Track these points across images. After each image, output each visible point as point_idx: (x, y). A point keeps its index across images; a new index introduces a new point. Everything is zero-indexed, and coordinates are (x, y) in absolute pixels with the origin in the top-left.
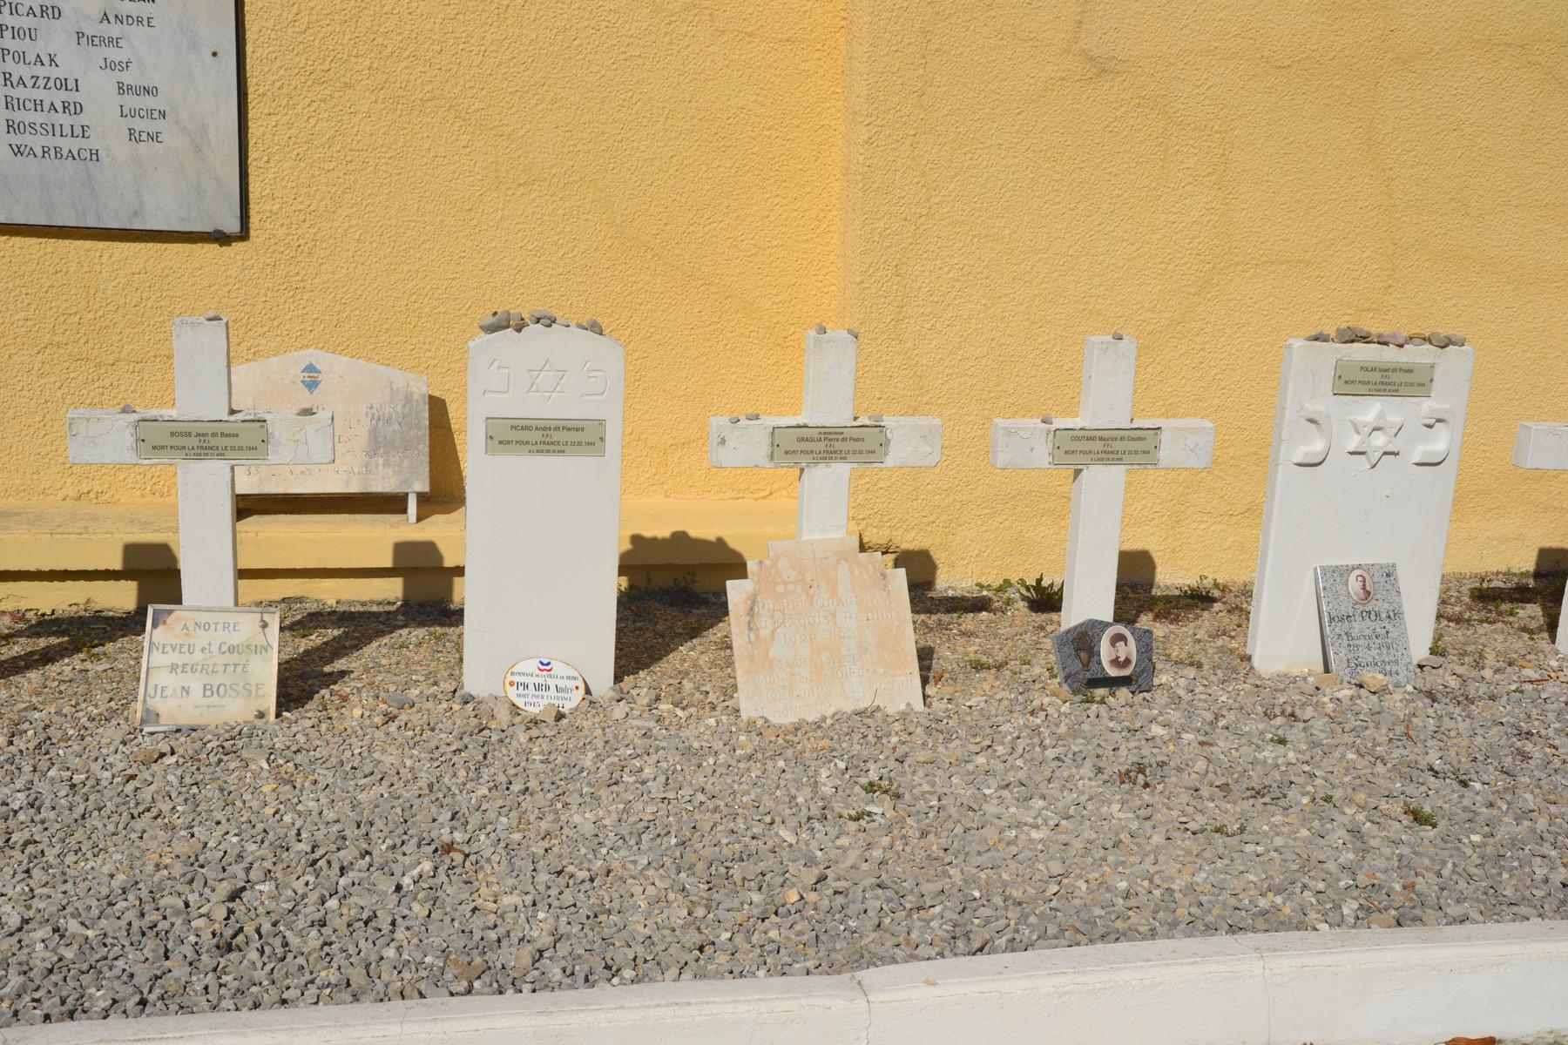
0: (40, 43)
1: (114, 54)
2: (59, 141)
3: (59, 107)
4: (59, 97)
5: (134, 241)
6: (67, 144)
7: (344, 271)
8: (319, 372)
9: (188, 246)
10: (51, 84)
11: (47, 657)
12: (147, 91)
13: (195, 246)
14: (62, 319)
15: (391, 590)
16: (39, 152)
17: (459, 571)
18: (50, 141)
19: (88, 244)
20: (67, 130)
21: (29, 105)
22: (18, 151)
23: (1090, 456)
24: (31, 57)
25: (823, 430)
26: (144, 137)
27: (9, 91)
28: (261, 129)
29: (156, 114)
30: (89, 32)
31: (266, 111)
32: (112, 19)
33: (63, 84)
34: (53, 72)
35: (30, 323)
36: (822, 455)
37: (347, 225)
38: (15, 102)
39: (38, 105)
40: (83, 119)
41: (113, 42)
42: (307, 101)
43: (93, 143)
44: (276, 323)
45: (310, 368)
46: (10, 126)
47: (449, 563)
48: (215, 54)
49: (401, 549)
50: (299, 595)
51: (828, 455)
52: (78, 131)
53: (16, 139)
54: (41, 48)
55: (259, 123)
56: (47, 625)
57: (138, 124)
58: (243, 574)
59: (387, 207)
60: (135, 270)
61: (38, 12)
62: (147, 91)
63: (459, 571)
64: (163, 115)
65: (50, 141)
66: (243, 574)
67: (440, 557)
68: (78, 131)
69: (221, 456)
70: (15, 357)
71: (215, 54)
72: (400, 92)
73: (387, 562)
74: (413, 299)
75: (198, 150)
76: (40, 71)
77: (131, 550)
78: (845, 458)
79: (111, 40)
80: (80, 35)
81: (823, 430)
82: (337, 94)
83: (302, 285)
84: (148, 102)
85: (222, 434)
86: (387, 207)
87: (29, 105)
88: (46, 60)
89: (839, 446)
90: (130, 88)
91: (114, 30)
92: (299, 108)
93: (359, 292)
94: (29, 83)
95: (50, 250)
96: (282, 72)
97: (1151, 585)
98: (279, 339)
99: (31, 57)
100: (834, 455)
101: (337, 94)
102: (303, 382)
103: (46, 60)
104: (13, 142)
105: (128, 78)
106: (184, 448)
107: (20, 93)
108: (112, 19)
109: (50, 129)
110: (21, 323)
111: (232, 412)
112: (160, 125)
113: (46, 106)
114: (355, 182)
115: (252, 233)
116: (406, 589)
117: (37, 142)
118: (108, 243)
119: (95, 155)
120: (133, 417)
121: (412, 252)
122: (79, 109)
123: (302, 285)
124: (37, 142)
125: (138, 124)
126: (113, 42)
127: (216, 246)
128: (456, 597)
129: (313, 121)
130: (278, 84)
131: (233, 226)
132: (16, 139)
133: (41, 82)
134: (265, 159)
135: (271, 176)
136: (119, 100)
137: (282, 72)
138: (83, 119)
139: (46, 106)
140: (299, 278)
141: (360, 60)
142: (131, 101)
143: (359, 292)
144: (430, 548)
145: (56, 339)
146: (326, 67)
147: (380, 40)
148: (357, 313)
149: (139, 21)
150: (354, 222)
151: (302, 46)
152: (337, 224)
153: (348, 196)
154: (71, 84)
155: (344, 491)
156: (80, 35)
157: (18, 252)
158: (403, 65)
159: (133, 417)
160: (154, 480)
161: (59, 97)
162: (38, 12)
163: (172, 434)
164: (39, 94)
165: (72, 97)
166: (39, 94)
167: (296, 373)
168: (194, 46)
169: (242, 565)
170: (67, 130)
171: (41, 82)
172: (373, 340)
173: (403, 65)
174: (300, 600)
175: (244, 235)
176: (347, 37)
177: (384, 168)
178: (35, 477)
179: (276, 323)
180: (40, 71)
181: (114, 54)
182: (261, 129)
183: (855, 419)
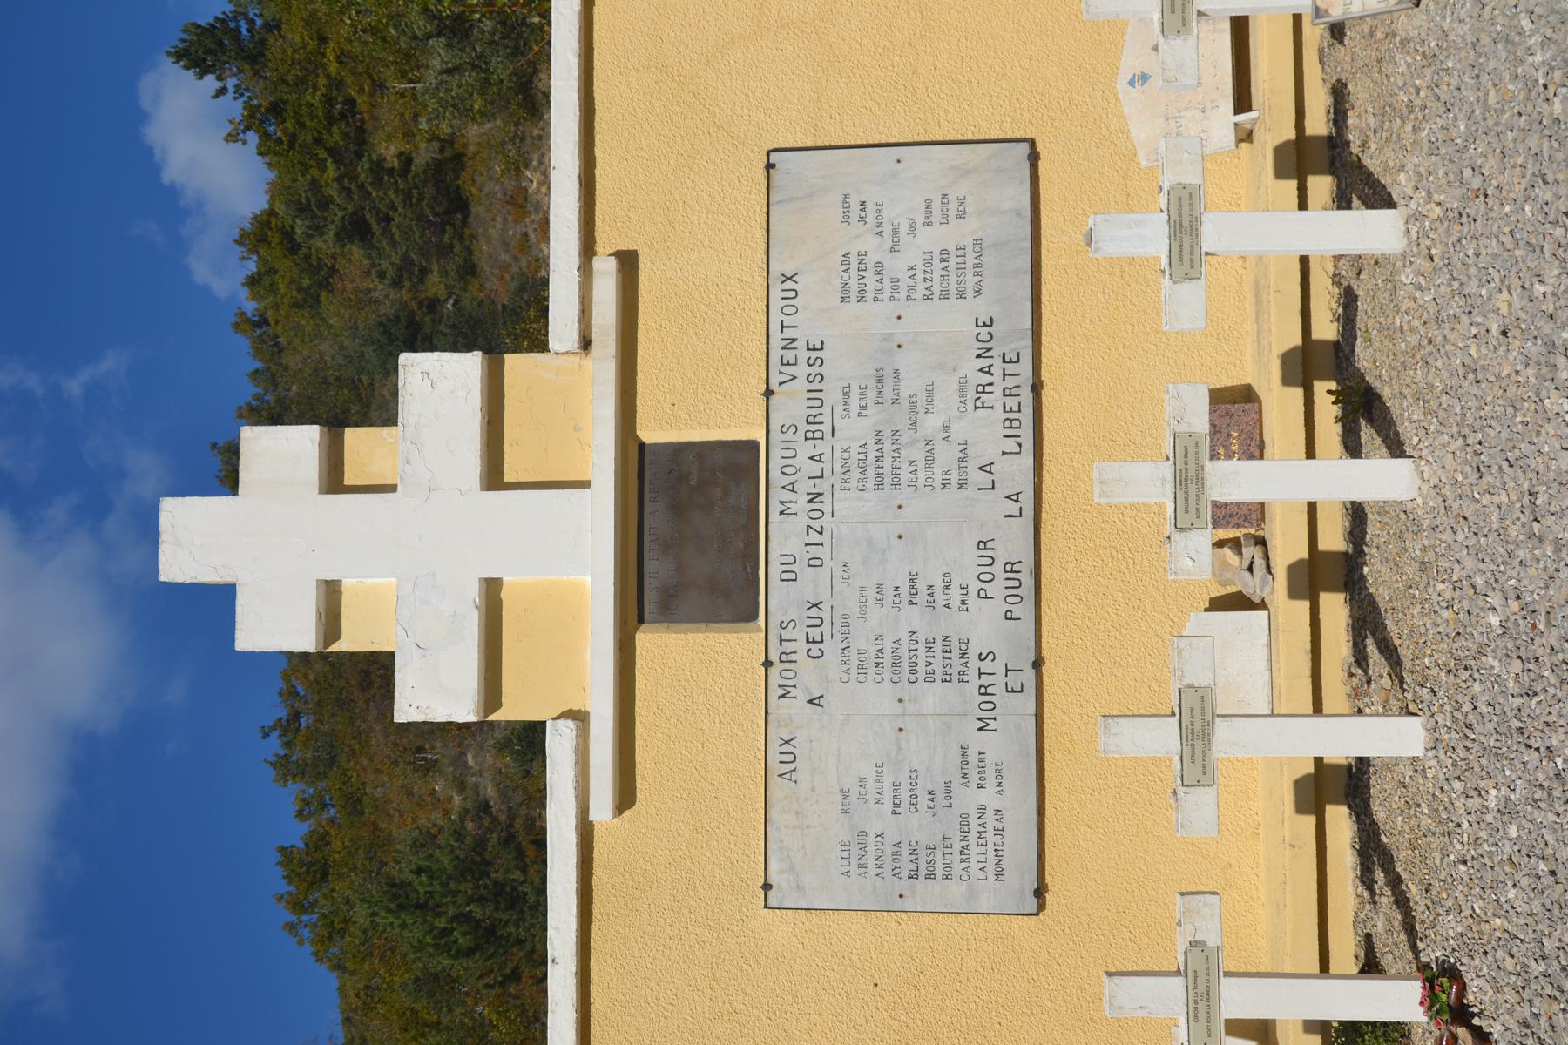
0: (900, 276)
1: (904, 229)
2: (969, 265)
3: (945, 264)
4: (937, 265)
5: (1039, 219)
6: (971, 260)
7: (1055, 69)
8: (1134, 75)
9: (1041, 182)
10: (928, 270)
11: (1395, 882)
12: (928, 206)
13: (1041, 178)
14: (1101, 269)
15: (1340, 820)
16: (978, 278)
17: (1318, 761)
18: (970, 272)
19: (1044, 251)
20: (961, 260)
21: (945, 284)
22: (978, 292)
23: (1195, 246)
24: (911, 282)
25: (1173, 238)
26: (961, 208)
27: (936, 296)
28: (951, 131)
29: (945, 201)
30: (890, 244)
31: (937, 128)
32: (880, 229)
33: (929, 262)
34: (920, 267)
35: (1106, 290)
36: (1206, 742)
37: (1019, 68)
38: (943, 293)
39: (944, 278)
40: (952, 249)
41: (895, 229)
42: (928, 99)
43: (969, 242)
44: (1098, 118)
45: (1132, 83)
46: (961, 296)
47: (1311, 769)
48: (899, 161)
49: (1293, 594)
50: (1316, 52)
51: (1200, 482)
52: (961, 253)
53: (970, 293)
54: (904, 276)
55: (946, 133)
56: (1367, 880)
57: (953, 212)
58: (1318, 709)
59: (1003, 39)
60: (1061, 219)
61: (879, 277)
62: (928, 206)
63: (1318, 761)
64: (945, 196)
65: (970, 272)
66: (1318, 709)
67: (1301, 562)
68: (961, 253)
69: (1211, 724)
70: (1133, 301)
71: (899, 161)
72: (918, 35)
73: (1306, 604)
74: (1074, 18)
75: (969, 172)
76: (920, 276)
77: (1301, 809)
78: (1202, 467)
79: (895, 230)
80: (892, 250)
81: (1173, 238)
82: (922, 79)
83: (1067, 100)
84: (936, 206)
85: (1186, 456)
86: (1003, 39)
87: (945, 284)
88: (912, 272)
89: (1192, 473)
90: (927, 218)
91: (887, 228)
92: (933, 105)
93: (1070, 58)
94: (929, 284)
95: (1050, 277)
96: (908, 118)
97: (1346, 553)
98: (1110, 116)
99: (911, 282)
100: (1200, 476)
101: (922, 79)
102: (1142, 84)
103: (912, 272)
104: (972, 295)
105: (920, 219)
106: (1197, 495)
107: (937, 290)
108: (880, 229)
109: (960, 271)
110: (1107, 296)
111: (1173, 714)
112: (952, 197)
113: (944, 273)
114: (985, 64)
115: (1029, 136)
116: (1332, 589)
117: (971, 280)
118: (1043, 238)
119: (977, 241)
120: (1180, 790)
121: (1037, 20)
122: (945, 252)
123: (1067, 100)
124: (971, 280)
125: (953, 212)
126: (895, 229)
127: (1040, 163)
128: (1345, 762)
129: (943, 96)
130: (917, 120)
131: (1024, 149)
132: (970, 293)
133: (928, 276)
134: (973, 128)
135: (985, 123)
136: (936, 225)
137: (908, 118)
138: (952, 249)
139: (944, 273)
140: (1062, 103)
141: (895, 64)
142: (937, 216)
143: (1070, 58)
144: (1292, 569)
145: (1117, 272)
146: (903, 88)
147: (880, 50)
148: (1086, 58)
149: (879, 211)
150: (1017, 64)
151: (888, 105)
152: (1019, 76)
153: (998, 69)
154: (928, 256)
155: (1229, 32)
156: (892, 250)
157: (1052, 298)
158: (898, 34)
159: (1180, 790)
160: (1227, 204)
161: (937, 265)
162: (880, 277)
163: (1187, 512)
164: (936, 277)
165: (936, 256)
166: (936, 277)
167: (1134, 93)
168: (894, 175)
169: (1316, 970)
170: (961, 260)
171: (928, 276)
172: (1108, 46)
173: (898, 34)
174: (1321, 51)
175: (1032, 142)
176: (879, 73)
177: (974, 43)
178: (1227, 289)
179: (1098, 118)
180: (920, 276)
181: (904, 229)
182: (951, 131)
183: (1162, 211)
